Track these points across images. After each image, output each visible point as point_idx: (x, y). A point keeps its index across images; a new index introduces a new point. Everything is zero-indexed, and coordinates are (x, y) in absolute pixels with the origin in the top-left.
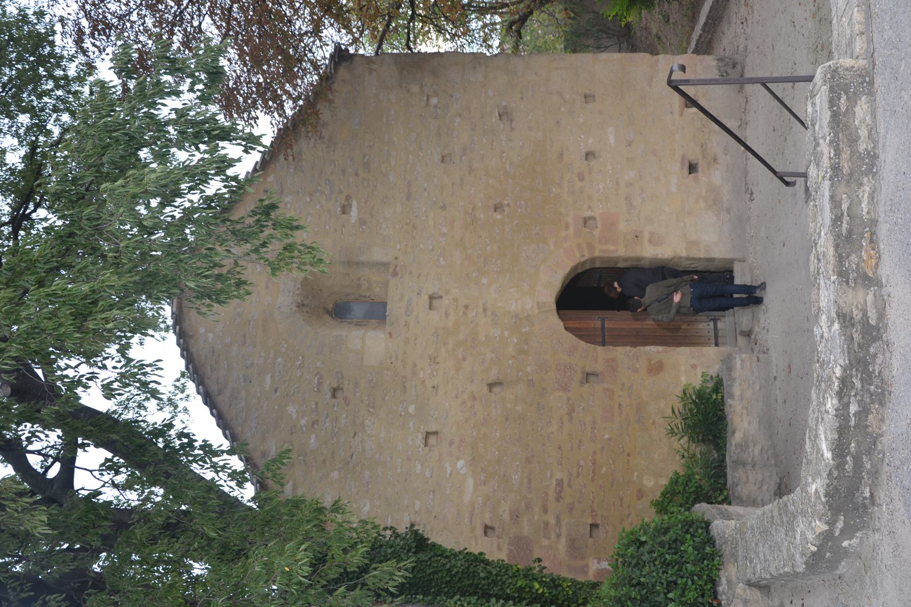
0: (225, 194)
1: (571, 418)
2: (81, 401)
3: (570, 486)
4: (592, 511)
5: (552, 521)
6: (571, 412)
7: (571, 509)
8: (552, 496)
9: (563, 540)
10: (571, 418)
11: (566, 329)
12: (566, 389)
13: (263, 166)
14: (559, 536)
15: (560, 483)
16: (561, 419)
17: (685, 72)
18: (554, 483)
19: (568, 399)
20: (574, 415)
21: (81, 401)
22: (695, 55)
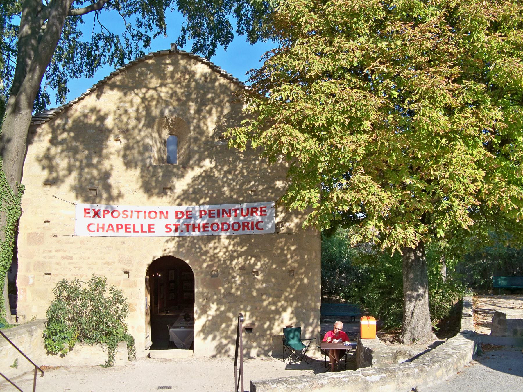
0: (454, 262)
1: (104, 264)
2: (508, 318)
3: (69, 263)
4: (57, 275)
5: (51, 254)
6: (107, 263)
7: (58, 264)
8: (64, 254)
9: (44, 260)
10: (104, 264)
11: (376, 334)
12: (120, 261)
13: (40, 24)
14: (45, 257)
15: (71, 258)
16: (104, 259)
17: (286, 369)
18: (71, 255)
19: (114, 262)
20: (106, 265)
21: (508, 318)
22: (48, 186)
